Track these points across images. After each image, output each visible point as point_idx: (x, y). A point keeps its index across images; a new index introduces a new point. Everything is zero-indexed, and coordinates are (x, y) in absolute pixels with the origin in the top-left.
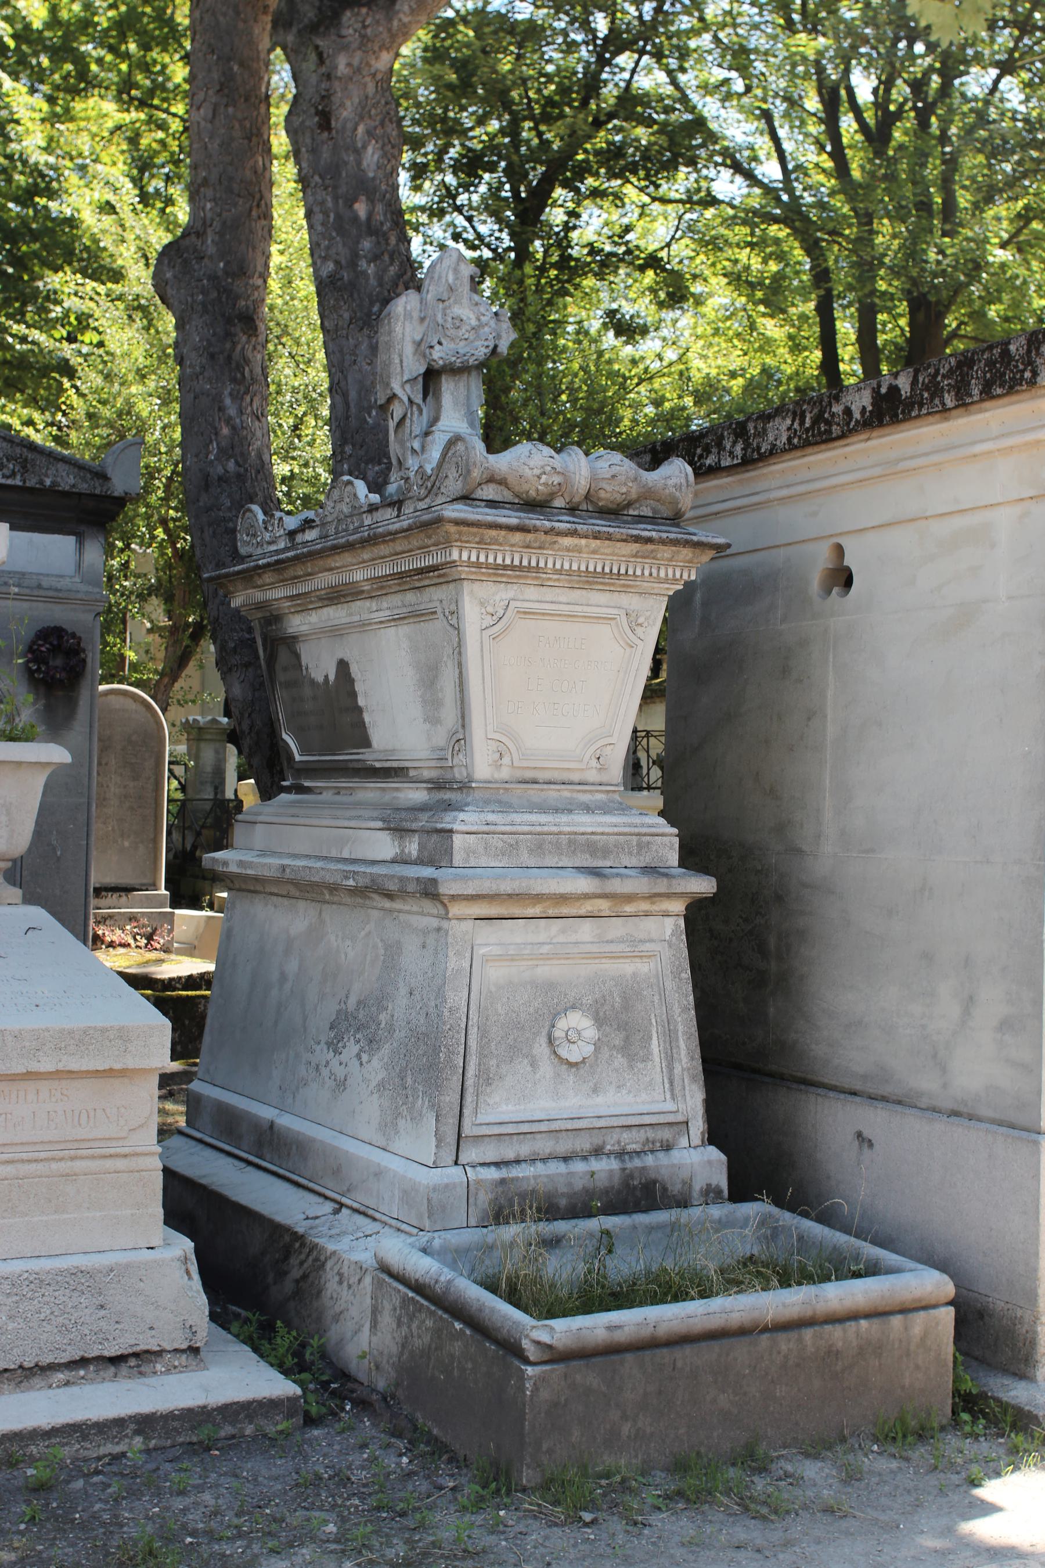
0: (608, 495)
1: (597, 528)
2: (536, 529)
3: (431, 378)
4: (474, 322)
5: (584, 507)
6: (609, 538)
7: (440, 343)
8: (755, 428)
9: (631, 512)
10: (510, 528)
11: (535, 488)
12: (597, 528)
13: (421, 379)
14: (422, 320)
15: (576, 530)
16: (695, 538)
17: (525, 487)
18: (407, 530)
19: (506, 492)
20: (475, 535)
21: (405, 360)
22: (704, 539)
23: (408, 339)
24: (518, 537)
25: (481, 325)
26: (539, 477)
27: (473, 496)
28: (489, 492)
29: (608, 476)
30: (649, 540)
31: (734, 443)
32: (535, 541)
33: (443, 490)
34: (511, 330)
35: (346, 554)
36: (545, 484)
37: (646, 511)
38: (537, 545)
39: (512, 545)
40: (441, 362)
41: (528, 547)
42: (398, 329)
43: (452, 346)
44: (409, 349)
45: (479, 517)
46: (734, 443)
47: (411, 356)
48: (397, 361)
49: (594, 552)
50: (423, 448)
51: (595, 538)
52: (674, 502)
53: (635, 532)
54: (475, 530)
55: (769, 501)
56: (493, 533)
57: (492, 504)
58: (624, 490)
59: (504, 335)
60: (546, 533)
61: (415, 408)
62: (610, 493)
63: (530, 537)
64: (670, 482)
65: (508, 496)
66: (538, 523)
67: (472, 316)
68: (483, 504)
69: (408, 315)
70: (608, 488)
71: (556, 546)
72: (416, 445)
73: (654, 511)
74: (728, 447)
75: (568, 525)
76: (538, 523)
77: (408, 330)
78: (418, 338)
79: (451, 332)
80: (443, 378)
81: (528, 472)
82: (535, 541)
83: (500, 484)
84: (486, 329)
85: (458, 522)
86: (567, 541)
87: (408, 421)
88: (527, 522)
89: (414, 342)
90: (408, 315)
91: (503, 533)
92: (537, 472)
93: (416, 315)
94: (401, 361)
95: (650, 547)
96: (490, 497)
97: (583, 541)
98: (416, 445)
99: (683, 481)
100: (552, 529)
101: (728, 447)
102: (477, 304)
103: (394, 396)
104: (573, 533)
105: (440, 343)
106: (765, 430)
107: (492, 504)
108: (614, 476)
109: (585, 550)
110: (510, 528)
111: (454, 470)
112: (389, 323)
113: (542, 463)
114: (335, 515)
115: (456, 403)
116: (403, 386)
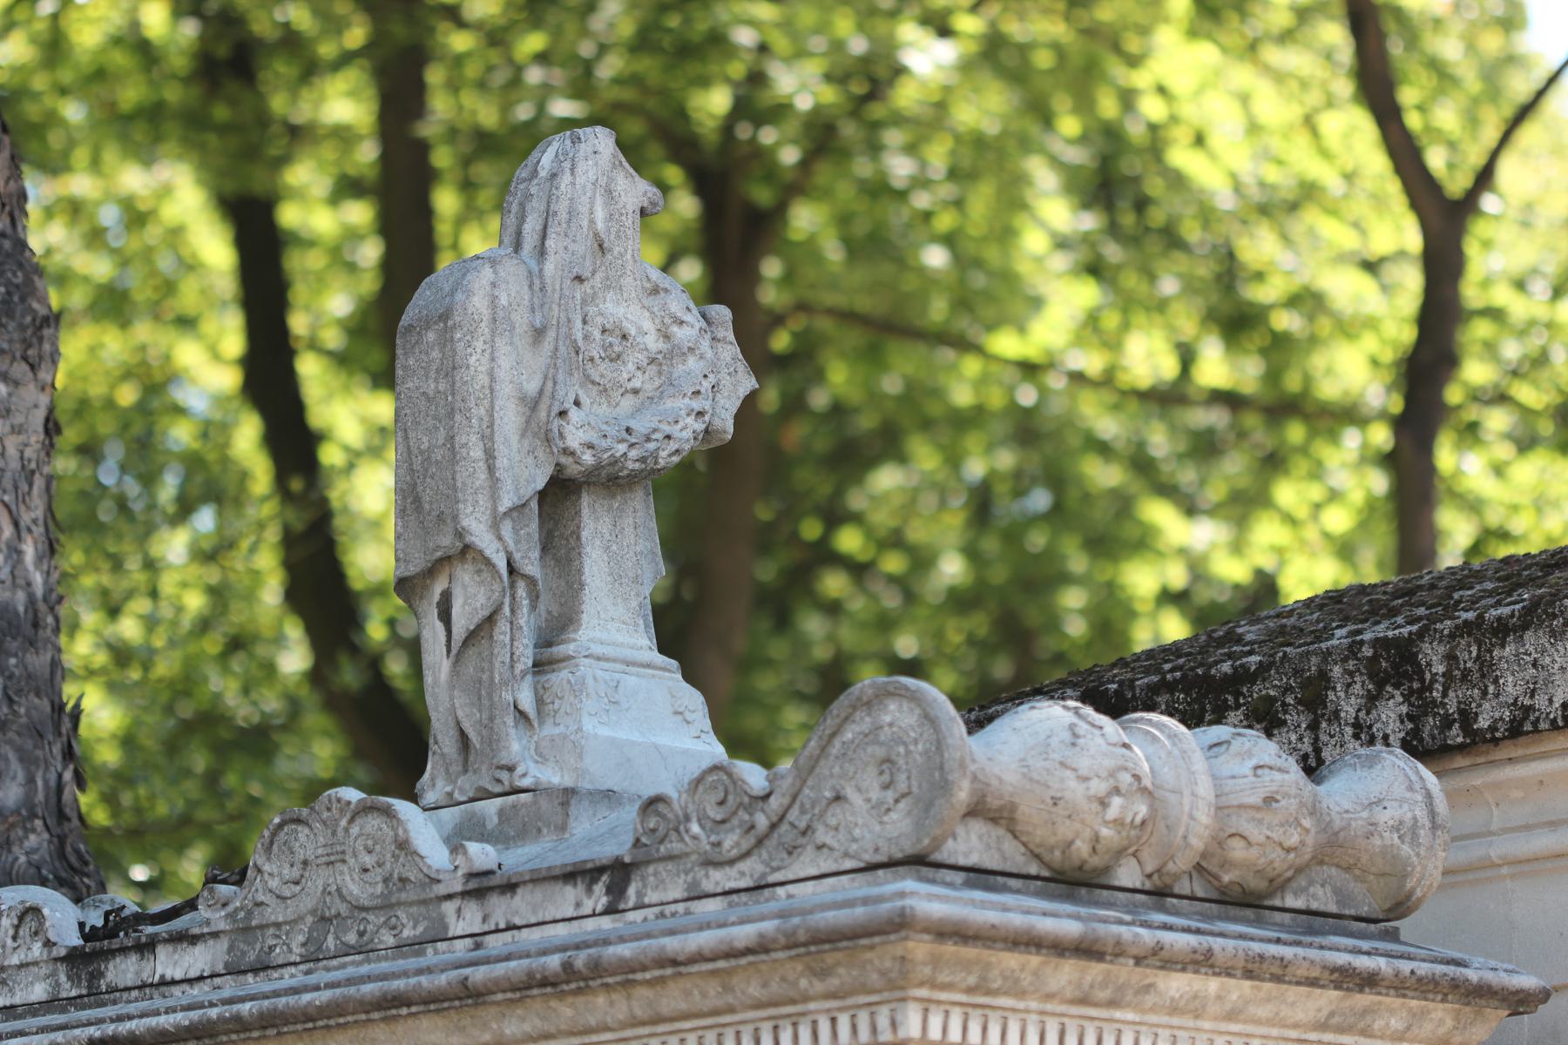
0: (1254, 853)
1: (1257, 947)
2: (1118, 951)
3: (560, 494)
4: (653, 343)
5: (1183, 887)
6: (1280, 974)
7: (577, 403)
8: (1451, 658)
9: (1291, 901)
10: (1059, 948)
11: (1082, 834)
12: (1257, 947)
13: (534, 505)
14: (539, 333)
15: (1209, 953)
16: (1472, 975)
17: (1065, 830)
18: (748, 951)
19: (1011, 846)
20: (967, 966)
21: (501, 450)
22: (1490, 977)
23: (505, 390)
24: (1066, 974)
25: (675, 353)
26: (1103, 803)
27: (937, 857)
28: (971, 844)
29: (1255, 799)
30: (1369, 981)
31: (1372, 700)
32: (1104, 985)
33: (822, 835)
34: (742, 366)
35: (425, 1022)
36: (1118, 823)
37: (1322, 899)
38: (1103, 995)
39: (1049, 997)
40: (588, 458)
41: (1084, 1001)
42: (477, 361)
43: (604, 410)
44: (509, 419)
45: (992, 917)
46: (1372, 700)
47: (514, 439)
48: (477, 453)
49: (1231, 1016)
50: (540, 702)
51: (1249, 974)
52: (1397, 870)
53: (1341, 959)
54: (970, 952)
55: (1488, 865)
56: (1011, 960)
57: (979, 876)
58: (1294, 840)
59: (726, 381)
60: (1139, 961)
61: (521, 591)
62: (1259, 848)
63: (1096, 970)
64: (1385, 817)
65: (1012, 855)
66: (1125, 932)
67: (647, 325)
68: (959, 877)
69: (498, 320)
70: (1256, 833)
71: (1150, 1000)
72: (526, 700)
73: (1341, 895)
74: (1349, 709)
75: (1192, 940)
76: (1125, 932)
77: (505, 362)
78: (532, 387)
79: (601, 371)
80: (586, 500)
81: (1074, 791)
82: (1104, 985)
83: (994, 820)
84: (692, 362)
85: (948, 932)
86: (1176, 984)
87: (502, 626)
88: (1101, 929)
89: (523, 399)
90: (498, 320)
91: (1034, 960)
92: (1099, 787)
93: (521, 319)
94: (490, 455)
95: (1364, 999)
96: (973, 860)
97: (1213, 985)
98: (526, 700)
99: (1421, 813)
100: (1158, 949)
101: (1349, 709)
102: (655, 291)
103: (466, 551)
104: (1202, 962)
105: (577, 403)
106: (1486, 667)
107: (979, 876)
108: (1269, 800)
109: (1213, 1009)
110: (1059, 948)
111: (871, 781)
112: (446, 340)
113: (1109, 763)
114: (308, 903)
115: (616, 578)
116: (495, 526)
